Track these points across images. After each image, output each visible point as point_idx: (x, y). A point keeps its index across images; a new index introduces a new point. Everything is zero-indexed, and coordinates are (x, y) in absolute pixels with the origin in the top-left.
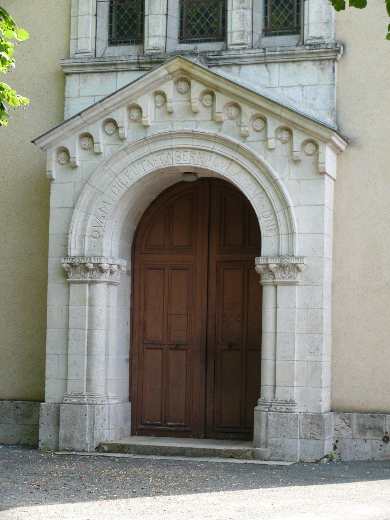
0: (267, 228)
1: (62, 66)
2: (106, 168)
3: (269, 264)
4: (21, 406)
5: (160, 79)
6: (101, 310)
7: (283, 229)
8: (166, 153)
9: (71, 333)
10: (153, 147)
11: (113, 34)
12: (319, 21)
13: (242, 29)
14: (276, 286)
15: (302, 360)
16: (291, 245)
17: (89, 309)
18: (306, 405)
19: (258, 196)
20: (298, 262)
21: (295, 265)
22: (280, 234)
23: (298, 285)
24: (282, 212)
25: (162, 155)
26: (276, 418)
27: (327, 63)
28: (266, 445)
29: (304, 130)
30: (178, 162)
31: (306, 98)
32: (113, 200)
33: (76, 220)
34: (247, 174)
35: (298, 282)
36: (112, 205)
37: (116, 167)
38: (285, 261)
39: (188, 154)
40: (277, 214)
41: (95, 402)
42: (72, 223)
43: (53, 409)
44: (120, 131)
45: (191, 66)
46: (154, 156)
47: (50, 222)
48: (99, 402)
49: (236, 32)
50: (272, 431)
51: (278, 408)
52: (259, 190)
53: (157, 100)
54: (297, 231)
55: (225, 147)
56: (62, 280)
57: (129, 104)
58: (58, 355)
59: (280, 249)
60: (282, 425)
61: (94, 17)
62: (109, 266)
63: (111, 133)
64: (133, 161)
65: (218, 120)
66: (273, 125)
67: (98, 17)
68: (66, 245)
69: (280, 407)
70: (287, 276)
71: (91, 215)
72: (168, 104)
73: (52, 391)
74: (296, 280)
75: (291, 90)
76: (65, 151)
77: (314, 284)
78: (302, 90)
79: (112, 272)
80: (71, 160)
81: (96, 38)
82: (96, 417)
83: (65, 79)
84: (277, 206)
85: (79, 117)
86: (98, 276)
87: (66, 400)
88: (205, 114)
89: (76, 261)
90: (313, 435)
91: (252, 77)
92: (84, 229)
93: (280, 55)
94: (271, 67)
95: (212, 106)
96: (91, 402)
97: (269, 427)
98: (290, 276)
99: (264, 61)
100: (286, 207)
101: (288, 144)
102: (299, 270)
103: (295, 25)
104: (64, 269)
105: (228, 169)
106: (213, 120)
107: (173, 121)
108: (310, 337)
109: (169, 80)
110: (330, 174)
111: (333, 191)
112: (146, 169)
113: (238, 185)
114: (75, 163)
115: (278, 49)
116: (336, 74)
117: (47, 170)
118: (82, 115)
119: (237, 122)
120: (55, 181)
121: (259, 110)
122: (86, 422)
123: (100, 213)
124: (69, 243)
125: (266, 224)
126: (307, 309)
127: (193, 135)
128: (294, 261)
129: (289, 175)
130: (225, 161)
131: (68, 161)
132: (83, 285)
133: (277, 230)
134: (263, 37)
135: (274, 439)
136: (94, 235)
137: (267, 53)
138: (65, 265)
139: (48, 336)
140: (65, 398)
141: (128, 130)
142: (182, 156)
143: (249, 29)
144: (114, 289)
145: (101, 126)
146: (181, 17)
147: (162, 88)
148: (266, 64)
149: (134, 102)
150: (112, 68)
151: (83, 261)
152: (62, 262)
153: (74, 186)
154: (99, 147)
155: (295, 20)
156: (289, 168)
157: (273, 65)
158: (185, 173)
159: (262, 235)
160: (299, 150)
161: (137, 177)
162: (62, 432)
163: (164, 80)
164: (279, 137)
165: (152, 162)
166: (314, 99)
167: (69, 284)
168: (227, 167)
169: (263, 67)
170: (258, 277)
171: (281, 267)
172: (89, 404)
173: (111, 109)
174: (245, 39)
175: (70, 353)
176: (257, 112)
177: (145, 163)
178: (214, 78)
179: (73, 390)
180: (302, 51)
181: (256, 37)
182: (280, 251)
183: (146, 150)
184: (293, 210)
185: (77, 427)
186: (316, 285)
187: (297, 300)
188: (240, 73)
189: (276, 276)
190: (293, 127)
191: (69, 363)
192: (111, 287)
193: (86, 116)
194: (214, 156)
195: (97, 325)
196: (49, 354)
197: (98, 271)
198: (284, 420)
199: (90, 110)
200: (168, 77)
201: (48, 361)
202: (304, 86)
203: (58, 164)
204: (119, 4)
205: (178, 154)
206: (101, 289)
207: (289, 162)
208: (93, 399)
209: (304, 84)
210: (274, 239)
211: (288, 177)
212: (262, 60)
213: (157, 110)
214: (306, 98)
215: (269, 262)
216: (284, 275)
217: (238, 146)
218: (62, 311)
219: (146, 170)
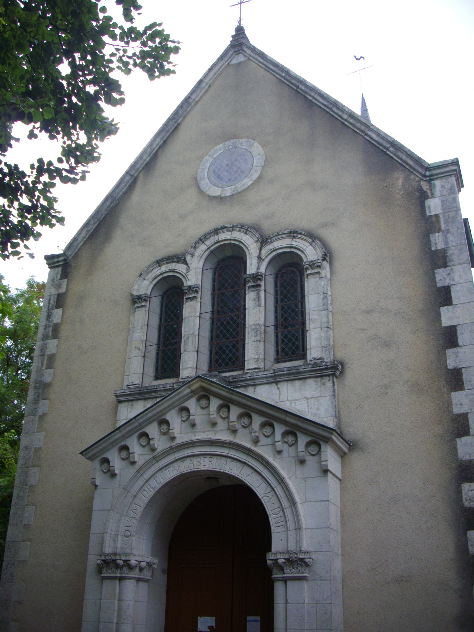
0: (277, 525)
1: (115, 396)
3: (278, 559)
6: (129, 605)
7: (291, 525)
12: (319, 345)
13: (257, 357)
16: (299, 542)
17: (119, 603)
19: (268, 495)
20: (305, 557)
21: (302, 560)
23: (307, 580)
25: (185, 462)
27: (327, 378)
31: (311, 409)
34: (258, 475)
35: (306, 576)
40: (285, 511)
44: (151, 442)
46: (179, 462)
52: (269, 489)
54: (304, 526)
59: (289, 544)
61: (143, 358)
62: (137, 563)
67: (146, 358)
72: (191, 418)
75: (298, 403)
77: (322, 578)
78: (307, 402)
79: (141, 569)
81: (143, 373)
83: (117, 408)
84: (285, 503)
86: (127, 572)
88: (222, 424)
91: (264, 393)
93: (287, 374)
94: (280, 385)
95: (228, 417)
98: (298, 571)
99: (275, 379)
100: (293, 503)
101: (293, 447)
102: (307, 565)
103: (301, 352)
106: (228, 429)
110: (334, 472)
111: (339, 490)
113: (250, 485)
114: (114, 470)
115: (285, 369)
116: (336, 387)
119: (249, 430)
126: (317, 604)
128: (302, 556)
130: (239, 464)
132: (114, 581)
134: (275, 364)
136: (126, 534)
137: (277, 373)
138: (99, 562)
141: (161, 444)
142: (202, 461)
143: (262, 357)
144: (143, 587)
146: (211, 354)
147: (187, 404)
148: (277, 383)
149: (164, 417)
150: (153, 395)
151: (114, 558)
154: (134, 456)
155: (301, 349)
157: (282, 383)
159: (272, 532)
160: (304, 450)
163: (187, 398)
164: (286, 440)
165: (177, 468)
166: (318, 409)
168: (240, 469)
169: (274, 385)
170: (269, 571)
174: (259, 365)
176: (266, 419)
178: (228, 392)
180: (305, 370)
181: (269, 364)
182: (289, 547)
183: (171, 458)
184: (299, 506)
186: (325, 580)
187: (306, 595)
188: (255, 392)
190: (298, 430)
192: (141, 584)
194: (229, 460)
195: (124, 619)
202: (309, 398)
204: (164, 349)
205: (198, 460)
206: (130, 585)
207: (295, 462)
209: (308, 397)
211: (294, 476)
212: (272, 380)
214: (311, 409)
216: (293, 570)
217: (250, 450)
219: (172, 475)
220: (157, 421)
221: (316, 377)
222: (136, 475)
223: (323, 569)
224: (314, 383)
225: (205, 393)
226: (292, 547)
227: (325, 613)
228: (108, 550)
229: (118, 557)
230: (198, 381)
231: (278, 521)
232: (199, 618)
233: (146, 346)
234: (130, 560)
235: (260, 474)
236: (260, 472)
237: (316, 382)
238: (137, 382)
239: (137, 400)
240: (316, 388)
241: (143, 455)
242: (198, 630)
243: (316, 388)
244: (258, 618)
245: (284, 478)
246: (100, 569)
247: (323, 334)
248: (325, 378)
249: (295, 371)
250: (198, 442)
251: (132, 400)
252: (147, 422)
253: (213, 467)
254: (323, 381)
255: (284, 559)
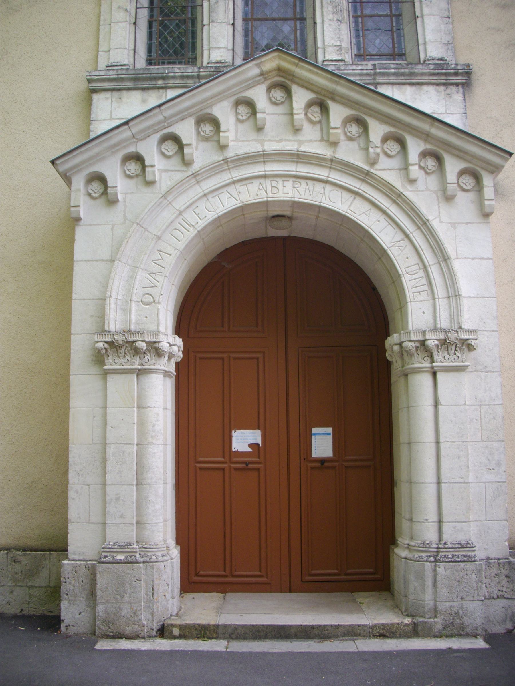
0: (415, 290)
2: (165, 201)
3: (403, 342)
4: (22, 559)
5: (248, 80)
8: (256, 182)
9: (111, 450)
10: (236, 174)
11: (154, 54)
14: (434, 374)
15: (478, 481)
16: (455, 313)
18: (487, 547)
19: (398, 244)
20: (470, 337)
22: (436, 297)
24: (437, 265)
25: (250, 186)
26: (448, 572)
27: (454, 89)
28: (435, 612)
29: (460, 154)
30: (275, 195)
32: (175, 249)
33: (117, 277)
36: (173, 255)
37: (181, 202)
38: (453, 336)
39: (289, 183)
41: (154, 558)
42: (111, 282)
43: (83, 571)
45: (294, 64)
46: (238, 185)
47: (74, 283)
48: (160, 559)
49: (330, 46)
50: (443, 592)
51: (450, 556)
52: (400, 236)
53: (240, 112)
55: (344, 175)
56: (95, 370)
57: (200, 113)
58: (88, 485)
60: (459, 581)
62: (168, 345)
63: (171, 154)
64: (205, 192)
65: (332, 139)
66: (415, 148)
68: (101, 316)
69: (452, 553)
70: (452, 357)
71: (140, 270)
73: (82, 542)
74: (466, 364)
76: (102, 179)
77: (487, 370)
80: (109, 190)
82: (156, 582)
83: (89, 103)
85: (126, 127)
86: (153, 361)
87: (106, 557)
89: (120, 339)
90: (501, 593)
92: (130, 291)
93: (394, 74)
96: (145, 559)
97: (439, 585)
98: (456, 358)
100: (443, 258)
104: (99, 351)
105: (350, 205)
107: (264, 141)
108: (487, 447)
109: (259, 84)
112: (225, 204)
117: (72, 204)
118: (131, 124)
119: (359, 144)
120: (82, 222)
121: (393, 126)
122: (140, 591)
123: (155, 268)
124: (107, 312)
125: (413, 282)
126: (480, 406)
127: (298, 157)
129: (439, 216)
130: (346, 195)
131: (105, 193)
132: (129, 376)
133: (429, 291)
135: (448, 604)
136: (145, 300)
137: (378, 71)
138: (100, 345)
139: (71, 455)
140: (104, 554)
142: (280, 186)
145: (156, 143)
147: (250, 94)
149: (208, 111)
150: (160, 83)
151: (131, 338)
152: (96, 340)
153: (112, 229)
154: (154, 172)
156: (439, 207)
158: (274, 217)
161: (211, 216)
162: (100, 608)
163: (253, 84)
164: (422, 165)
165: (235, 195)
167: (106, 373)
168: (349, 203)
171: (444, 343)
172: (144, 562)
173: (173, 119)
175: (109, 481)
176: (392, 129)
177: (224, 196)
178: (331, 80)
179: (115, 541)
180: (424, 71)
183: (226, 177)
185: (127, 599)
189: (436, 357)
191: (108, 498)
193: (136, 127)
194: (328, 188)
195: (152, 437)
196: (74, 484)
197: (153, 354)
198: (461, 574)
199: (142, 118)
200: (258, 79)
201: (71, 494)
203: (87, 198)
205: (274, 184)
207: (438, 199)
208: (149, 554)
210: (427, 306)
211: (438, 219)
213: (240, 126)
215: (427, 338)
218: (94, 417)
219: (226, 206)
220: (195, 116)
221: (438, 85)
222: (160, 203)
223: (488, 356)
224: (436, 93)
225: (283, 79)
226: (444, 322)
227: (494, 418)
228: (114, 323)
229: (139, 338)
230: (274, 58)
231: (417, 285)
232: (233, 431)
233: (137, 8)
234: (159, 342)
235: (384, 212)
236: (385, 208)
237: (438, 91)
238: (126, 62)
239: (129, 89)
240: (439, 101)
241: (167, 171)
242: (233, 450)
243: (439, 101)
244: (330, 430)
245: (428, 220)
246: (99, 358)
247: (443, 27)
248: (451, 87)
249: (407, 71)
250: (275, 154)
251: (119, 90)
252: (179, 117)
253: (300, 196)
254: (449, 91)
255: (437, 340)
